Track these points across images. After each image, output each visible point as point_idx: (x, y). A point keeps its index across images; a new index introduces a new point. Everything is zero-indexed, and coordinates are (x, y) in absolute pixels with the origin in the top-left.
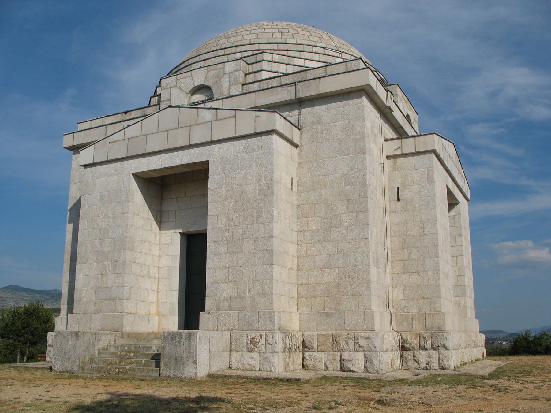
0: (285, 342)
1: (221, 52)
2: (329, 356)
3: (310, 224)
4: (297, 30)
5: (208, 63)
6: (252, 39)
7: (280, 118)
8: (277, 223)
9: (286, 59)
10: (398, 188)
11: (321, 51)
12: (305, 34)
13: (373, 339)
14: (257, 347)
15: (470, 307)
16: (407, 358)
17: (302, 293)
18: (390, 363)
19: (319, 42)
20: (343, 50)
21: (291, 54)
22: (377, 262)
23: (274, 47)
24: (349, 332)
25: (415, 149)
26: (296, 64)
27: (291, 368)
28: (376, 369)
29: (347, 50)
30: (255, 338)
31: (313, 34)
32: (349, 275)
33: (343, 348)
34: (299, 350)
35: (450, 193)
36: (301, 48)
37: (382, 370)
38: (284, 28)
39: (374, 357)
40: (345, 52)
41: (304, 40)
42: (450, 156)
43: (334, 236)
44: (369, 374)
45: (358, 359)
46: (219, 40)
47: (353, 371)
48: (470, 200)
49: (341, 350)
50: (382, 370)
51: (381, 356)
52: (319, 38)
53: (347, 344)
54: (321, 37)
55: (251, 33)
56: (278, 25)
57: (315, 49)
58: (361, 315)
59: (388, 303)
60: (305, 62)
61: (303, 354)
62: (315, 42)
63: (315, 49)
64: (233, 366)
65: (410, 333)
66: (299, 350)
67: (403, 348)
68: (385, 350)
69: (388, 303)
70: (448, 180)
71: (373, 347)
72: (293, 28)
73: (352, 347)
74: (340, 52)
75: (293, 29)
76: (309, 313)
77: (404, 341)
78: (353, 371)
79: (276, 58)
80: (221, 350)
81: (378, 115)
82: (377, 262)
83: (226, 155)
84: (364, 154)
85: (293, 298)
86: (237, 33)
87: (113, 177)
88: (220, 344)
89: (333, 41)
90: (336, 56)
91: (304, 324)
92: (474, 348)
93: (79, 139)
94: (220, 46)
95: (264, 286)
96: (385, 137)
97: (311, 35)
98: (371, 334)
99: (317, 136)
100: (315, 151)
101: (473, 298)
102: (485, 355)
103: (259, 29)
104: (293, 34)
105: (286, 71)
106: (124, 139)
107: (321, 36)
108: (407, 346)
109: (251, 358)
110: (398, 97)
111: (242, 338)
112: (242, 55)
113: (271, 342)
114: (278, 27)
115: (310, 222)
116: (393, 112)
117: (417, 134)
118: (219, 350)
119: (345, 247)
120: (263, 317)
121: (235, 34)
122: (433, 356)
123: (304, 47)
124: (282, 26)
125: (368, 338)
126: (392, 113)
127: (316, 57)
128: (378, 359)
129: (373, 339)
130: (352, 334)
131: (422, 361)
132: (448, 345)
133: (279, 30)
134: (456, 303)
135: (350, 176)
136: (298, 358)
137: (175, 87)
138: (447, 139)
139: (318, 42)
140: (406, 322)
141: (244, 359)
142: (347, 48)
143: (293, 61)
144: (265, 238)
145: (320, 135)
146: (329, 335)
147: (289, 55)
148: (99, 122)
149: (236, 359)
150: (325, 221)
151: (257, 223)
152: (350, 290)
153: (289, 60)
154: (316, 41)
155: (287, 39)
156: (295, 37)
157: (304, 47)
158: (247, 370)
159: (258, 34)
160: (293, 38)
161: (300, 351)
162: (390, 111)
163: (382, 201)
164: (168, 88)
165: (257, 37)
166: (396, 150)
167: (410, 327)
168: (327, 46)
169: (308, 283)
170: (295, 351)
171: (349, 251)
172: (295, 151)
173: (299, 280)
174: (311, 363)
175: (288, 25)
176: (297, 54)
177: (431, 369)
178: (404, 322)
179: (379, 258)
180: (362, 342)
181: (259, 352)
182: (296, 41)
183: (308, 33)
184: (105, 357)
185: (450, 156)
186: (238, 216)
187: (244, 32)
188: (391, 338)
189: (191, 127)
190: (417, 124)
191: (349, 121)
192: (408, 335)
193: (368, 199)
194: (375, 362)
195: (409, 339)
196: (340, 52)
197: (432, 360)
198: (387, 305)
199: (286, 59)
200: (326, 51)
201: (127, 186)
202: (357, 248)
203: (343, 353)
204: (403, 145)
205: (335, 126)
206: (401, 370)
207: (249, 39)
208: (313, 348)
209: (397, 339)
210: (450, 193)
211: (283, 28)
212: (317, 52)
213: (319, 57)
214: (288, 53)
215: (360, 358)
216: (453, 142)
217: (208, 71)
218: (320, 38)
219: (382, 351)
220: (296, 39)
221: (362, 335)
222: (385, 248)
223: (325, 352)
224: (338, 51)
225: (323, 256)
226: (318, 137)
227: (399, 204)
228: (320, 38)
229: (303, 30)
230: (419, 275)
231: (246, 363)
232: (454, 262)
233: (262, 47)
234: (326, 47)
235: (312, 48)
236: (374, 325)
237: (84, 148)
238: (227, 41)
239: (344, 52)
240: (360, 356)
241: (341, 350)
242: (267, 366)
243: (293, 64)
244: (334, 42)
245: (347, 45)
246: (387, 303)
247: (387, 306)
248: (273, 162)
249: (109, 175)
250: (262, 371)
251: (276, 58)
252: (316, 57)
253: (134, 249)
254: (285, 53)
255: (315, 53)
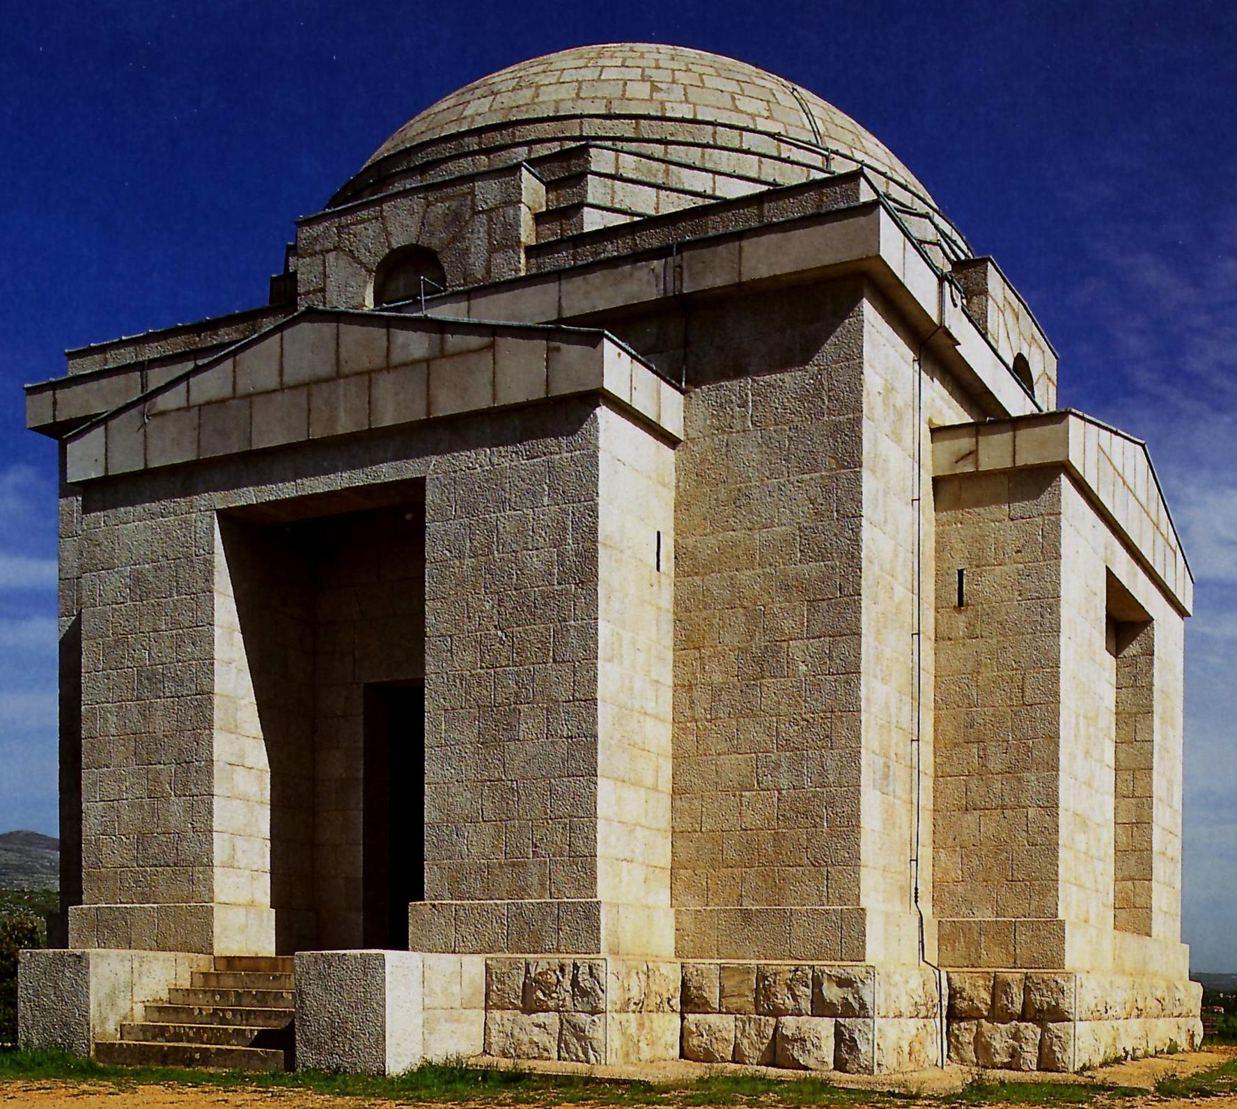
0: (626, 985)
1: (473, 143)
2: (748, 1026)
3: (707, 667)
4: (700, 75)
5: (433, 177)
6: (563, 100)
7: (619, 354)
8: (610, 660)
9: (657, 172)
10: (961, 573)
11: (769, 146)
12: (723, 89)
13: (860, 985)
14: (552, 998)
15: (1165, 908)
16: (960, 1038)
17: (683, 856)
18: (906, 1049)
19: (763, 117)
20: (832, 145)
21: (676, 153)
22: (886, 777)
23: (625, 128)
24: (798, 962)
25: (1014, 461)
26: (687, 187)
27: (646, 1053)
28: (864, 1063)
29: (850, 147)
30: (547, 974)
31: (748, 89)
32: (806, 811)
33: (783, 1004)
34: (671, 1007)
35: (1115, 589)
36: (705, 135)
37: (879, 1065)
38: (660, 68)
39: (860, 1030)
40: (840, 151)
41: (719, 108)
42: (1124, 483)
43: (769, 702)
44: (846, 1076)
45: (818, 1035)
46: (469, 102)
47: (806, 1068)
48: (1191, 613)
49: (777, 1013)
50: (879, 1065)
51: (880, 1030)
52: (765, 103)
53: (795, 997)
54: (772, 99)
55: (561, 81)
56: (646, 55)
57: (749, 140)
58: (834, 918)
59: (916, 889)
60: (714, 183)
61: (683, 1019)
62: (752, 116)
63: (749, 140)
64: (494, 1047)
65: (971, 972)
66: (671, 1007)
67: (953, 1015)
68: (891, 1015)
69: (916, 889)
70: (1113, 553)
71: (856, 1006)
72: (688, 67)
73: (805, 1005)
74: (827, 150)
75: (689, 70)
76: (700, 911)
77: (956, 993)
78: (806, 1068)
79: (629, 165)
80: (457, 1005)
81: (910, 355)
82: (886, 777)
83: (472, 463)
84: (858, 469)
85: (657, 870)
86: (520, 77)
87: (166, 519)
88: (456, 989)
89: (806, 114)
90: (812, 163)
91: (686, 938)
92: (1162, 1019)
93: (74, 403)
94: (469, 119)
95: (572, 834)
96: (934, 421)
97: (743, 95)
98: (856, 971)
99: (731, 413)
100: (724, 457)
101: (1178, 886)
102: (1198, 1040)
103: (586, 66)
104: (685, 89)
105: (657, 209)
106: (188, 408)
107: (774, 95)
108: (962, 1005)
109: (538, 1026)
110: (990, 299)
111: (515, 972)
112: (530, 151)
113: (588, 985)
114: (643, 63)
115: (706, 662)
116: (959, 344)
117: (1040, 410)
118: (454, 1006)
119: (795, 734)
120: (569, 918)
121: (514, 82)
122: (1029, 1034)
123: (715, 133)
124: (657, 60)
125: (844, 983)
126: (957, 347)
127: (750, 165)
128: (870, 1037)
129: (860, 985)
130: (807, 967)
131: (998, 1047)
132: (1066, 1006)
133: (646, 73)
134: (1125, 896)
135: (815, 533)
136: (668, 1026)
137: (335, 249)
138: (1119, 431)
139: (760, 116)
140: (964, 942)
141: (521, 1029)
142: (849, 138)
143: (679, 178)
144: (577, 703)
145: (738, 409)
146: (747, 971)
147: (669, 157)
148: (127, 356)
149: (501, 1028)
150: (747, 660)
151: (555, 661)
152: (807, 852)
153: (667, 172)
154: (757, 113)
155: (668, 105)
156: (691, 99)
157: (715, 133)
158: (529, 1058)
159: (580, 83)
160: (687, 101)
161: (673, 1011)
162: (950, 342)
163: (908, 606)
164: (316, 253)
165: (578, 94)
166: (962, 458)
167: (973, 955)
168: (786, 131)
169: (698, 829)
170: (659, 1008)
171: (806, 744)
172: (669, 454)
173: (678, 820)
174: (702, 1042)
175: (676, 58)
176: (694, 155)
177: (1019, 1069)
178: (959, 942)
179: (891, 768)
180: (832, 993)
181: (559, 1011)
182: (695, 111)
183: (732, 87)
184: (204, 1021)
185: (1124, 483)
186: (504, 638)
187: (543, 75)
188: (915, 983)
189: (373, 376)
190: (1051, 384)
191: (820, 369)
192: (966, 976)
193: (861, 599)
194: (863, 1047)
195: (967, 988)
196: (827, 150)
197: (1024, 1046)
198: (913, 895)
199: (657, 172)
200: (782, 148)
201: (206, 548)
202: (827, 737)
203: (783, 1019)
204: (980, 448)
205: (781, 384)
206: (942, 1068)
207: (554, 101)
208: (707, 1003)
209: (932, 985)
210: (1115, 589)
211: (658, 68)
212: (753, 149)
213: (760, 167)
214: (666, 152)
215: (824, 1034)
216: (1143, 442)
217: (429, 204)
218: (768, 102)
219: (882, 1017)
220: (695, 105)
221: (833, 973)
222: (912, 740)
223: (738, 1016)
224: (819, 148)
225: (740, 756)
226: (732, 417)
227: (961, 621)
228: (768, 102)
229: (719, 75)
230: (1005, 817)
231: (526, 1039)
232: (1127, 787)
233: (590, 128)
234: (783, 133)
235: (741, 136)
236: (864, 947)
237: (1132, 438)
238: (491, 106)
239: (837, 153)
240: (826, 1026)
241: (777, 1013)
242: (577, 1049)
243: (679, 186)
244: (810, 116)
245: (851, 128)
246: (913, 891)
247: (913, 899)
248: (597, 485)
249: (153, 514)
250: (565, 1059)
251: (629, 165)
252: (750, 165)
253: (236, 726)
254: (658, 150)
255: (748, 152)
